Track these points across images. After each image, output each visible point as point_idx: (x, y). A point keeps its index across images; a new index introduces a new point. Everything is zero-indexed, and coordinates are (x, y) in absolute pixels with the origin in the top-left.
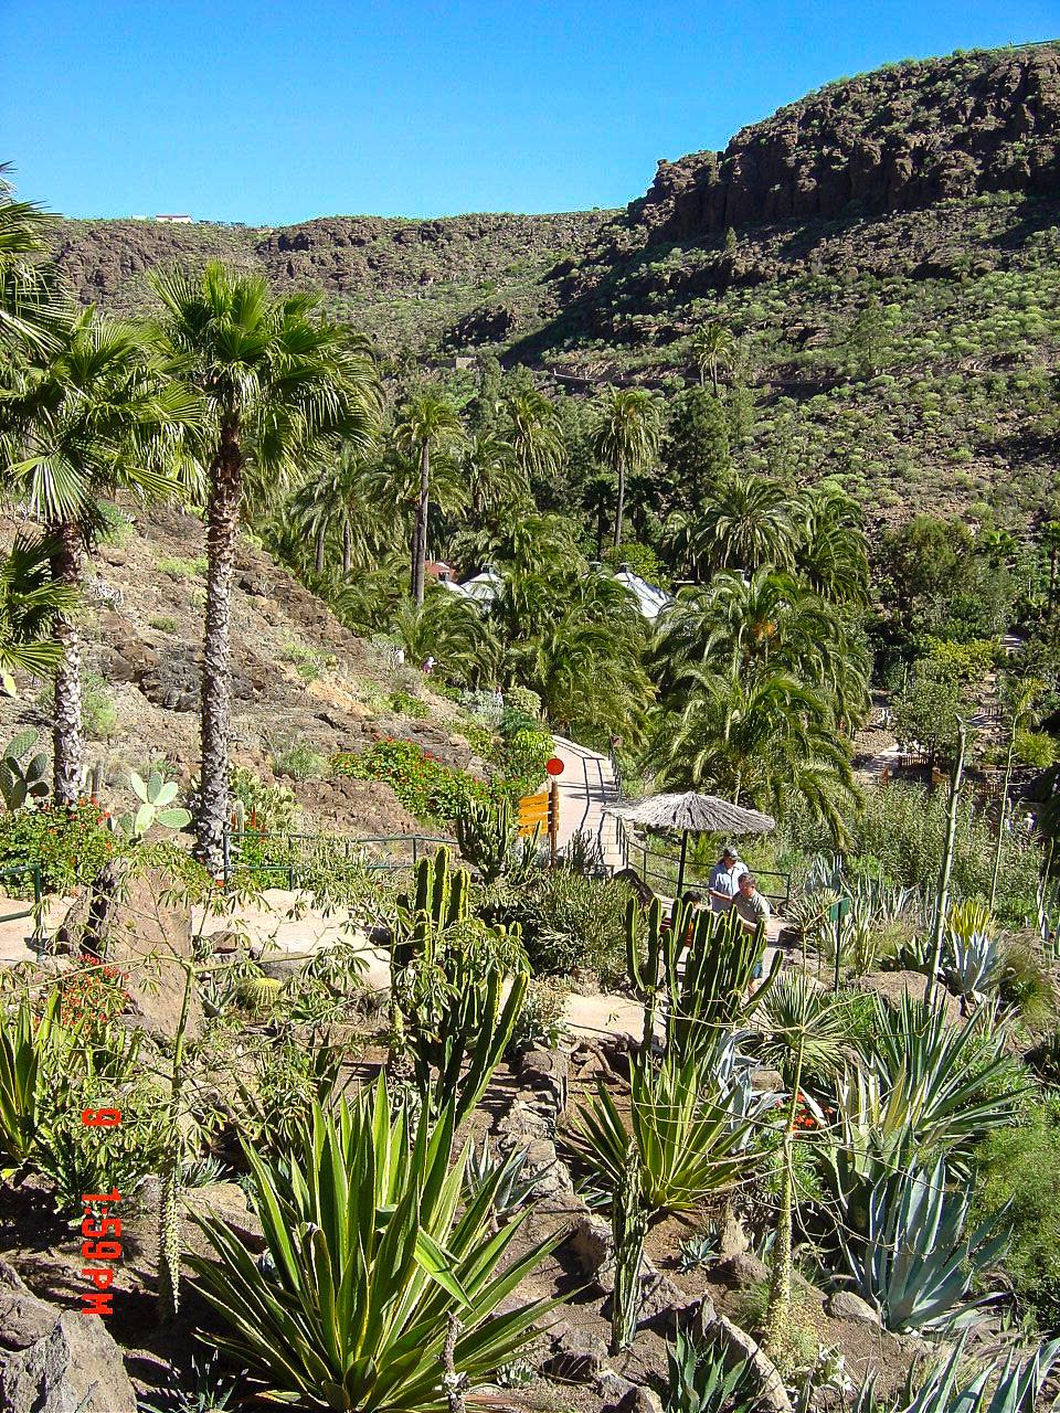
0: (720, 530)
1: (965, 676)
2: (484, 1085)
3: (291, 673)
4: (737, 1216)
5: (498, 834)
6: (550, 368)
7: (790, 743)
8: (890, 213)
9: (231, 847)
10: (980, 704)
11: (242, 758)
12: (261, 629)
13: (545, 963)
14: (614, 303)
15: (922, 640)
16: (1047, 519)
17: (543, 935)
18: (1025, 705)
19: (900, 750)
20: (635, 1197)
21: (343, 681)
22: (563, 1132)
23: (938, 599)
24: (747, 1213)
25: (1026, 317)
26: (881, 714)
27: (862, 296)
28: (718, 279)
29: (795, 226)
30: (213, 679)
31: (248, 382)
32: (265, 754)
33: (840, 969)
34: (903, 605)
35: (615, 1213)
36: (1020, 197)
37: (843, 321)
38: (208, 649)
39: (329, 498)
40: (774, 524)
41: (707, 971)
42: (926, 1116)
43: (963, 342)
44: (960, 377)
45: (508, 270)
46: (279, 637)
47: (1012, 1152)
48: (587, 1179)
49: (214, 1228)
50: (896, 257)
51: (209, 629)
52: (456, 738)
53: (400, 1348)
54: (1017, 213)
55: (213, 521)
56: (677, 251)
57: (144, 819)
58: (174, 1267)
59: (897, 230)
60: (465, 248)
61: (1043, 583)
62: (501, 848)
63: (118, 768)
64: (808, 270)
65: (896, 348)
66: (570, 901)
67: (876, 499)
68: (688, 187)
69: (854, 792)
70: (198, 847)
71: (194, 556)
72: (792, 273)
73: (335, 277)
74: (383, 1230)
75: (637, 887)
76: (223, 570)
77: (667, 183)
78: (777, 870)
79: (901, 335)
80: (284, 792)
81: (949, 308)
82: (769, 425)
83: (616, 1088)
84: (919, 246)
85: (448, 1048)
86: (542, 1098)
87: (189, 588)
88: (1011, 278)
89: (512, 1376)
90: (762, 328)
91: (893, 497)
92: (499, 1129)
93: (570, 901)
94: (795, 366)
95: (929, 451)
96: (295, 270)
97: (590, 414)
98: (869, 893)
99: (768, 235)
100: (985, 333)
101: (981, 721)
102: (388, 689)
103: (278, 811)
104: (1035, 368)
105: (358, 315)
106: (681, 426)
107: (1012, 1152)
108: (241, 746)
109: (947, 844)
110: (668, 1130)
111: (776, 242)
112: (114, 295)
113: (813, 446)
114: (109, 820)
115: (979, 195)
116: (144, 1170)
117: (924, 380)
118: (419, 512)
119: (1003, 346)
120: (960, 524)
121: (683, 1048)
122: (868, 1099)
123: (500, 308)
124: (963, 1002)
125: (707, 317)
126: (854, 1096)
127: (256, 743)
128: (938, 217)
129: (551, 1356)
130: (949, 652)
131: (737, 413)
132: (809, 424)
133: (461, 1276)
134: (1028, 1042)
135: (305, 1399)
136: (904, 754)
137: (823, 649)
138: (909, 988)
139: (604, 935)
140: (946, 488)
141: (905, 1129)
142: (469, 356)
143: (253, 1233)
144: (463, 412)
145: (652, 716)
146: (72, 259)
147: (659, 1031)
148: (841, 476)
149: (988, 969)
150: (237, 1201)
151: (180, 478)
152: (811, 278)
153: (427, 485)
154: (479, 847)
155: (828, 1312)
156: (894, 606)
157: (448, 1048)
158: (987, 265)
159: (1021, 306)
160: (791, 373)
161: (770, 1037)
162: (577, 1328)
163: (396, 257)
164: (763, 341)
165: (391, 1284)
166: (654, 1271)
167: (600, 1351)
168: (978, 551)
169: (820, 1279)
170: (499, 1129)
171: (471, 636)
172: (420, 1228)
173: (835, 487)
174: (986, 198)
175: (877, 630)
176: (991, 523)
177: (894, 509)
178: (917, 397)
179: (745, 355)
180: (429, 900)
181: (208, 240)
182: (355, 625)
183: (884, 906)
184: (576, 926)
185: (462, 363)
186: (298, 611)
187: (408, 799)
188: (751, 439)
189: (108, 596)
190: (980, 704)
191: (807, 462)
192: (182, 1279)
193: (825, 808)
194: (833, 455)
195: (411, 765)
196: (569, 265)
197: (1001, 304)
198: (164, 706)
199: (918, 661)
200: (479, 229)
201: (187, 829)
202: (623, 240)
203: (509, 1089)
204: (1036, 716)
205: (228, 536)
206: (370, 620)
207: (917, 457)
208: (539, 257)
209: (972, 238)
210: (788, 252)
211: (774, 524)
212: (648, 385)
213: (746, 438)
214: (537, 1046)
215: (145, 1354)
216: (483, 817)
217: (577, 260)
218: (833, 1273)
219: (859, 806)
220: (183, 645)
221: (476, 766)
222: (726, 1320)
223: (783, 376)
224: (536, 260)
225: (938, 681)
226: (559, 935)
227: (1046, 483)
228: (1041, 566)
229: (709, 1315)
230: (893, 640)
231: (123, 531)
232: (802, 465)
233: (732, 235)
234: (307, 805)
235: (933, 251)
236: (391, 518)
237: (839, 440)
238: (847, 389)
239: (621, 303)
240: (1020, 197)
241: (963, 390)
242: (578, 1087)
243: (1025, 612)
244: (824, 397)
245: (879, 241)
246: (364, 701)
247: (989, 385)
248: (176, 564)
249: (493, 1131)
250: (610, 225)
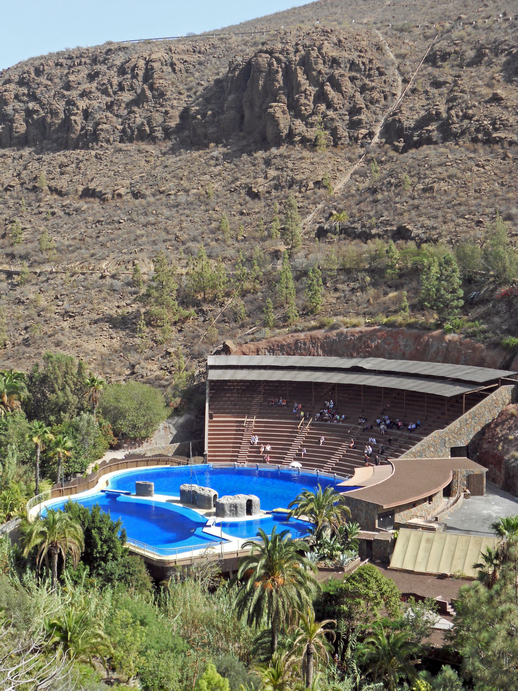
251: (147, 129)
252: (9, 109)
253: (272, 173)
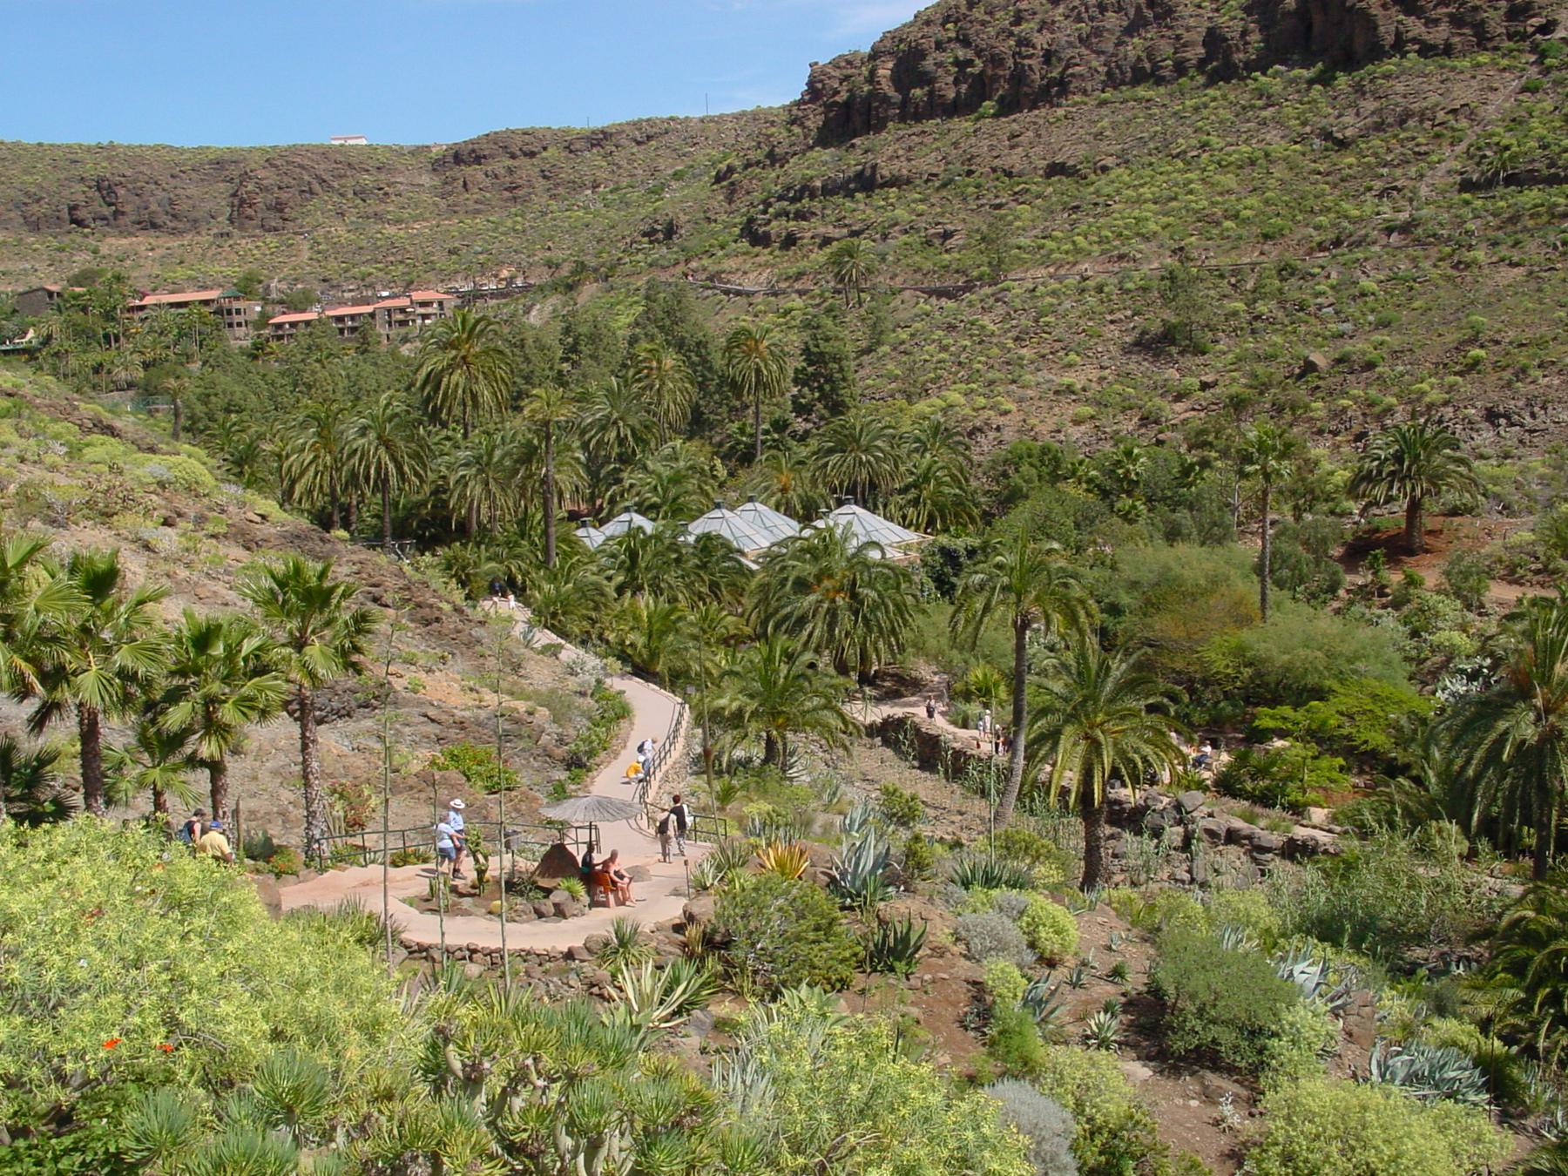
90: (906, 232)
96: (470, 185)
146: (250, 187)
158: (1109, 161)
200: (647, 134)
251: (1147, 66)
252: (928, 64)
253: (1369, 105)
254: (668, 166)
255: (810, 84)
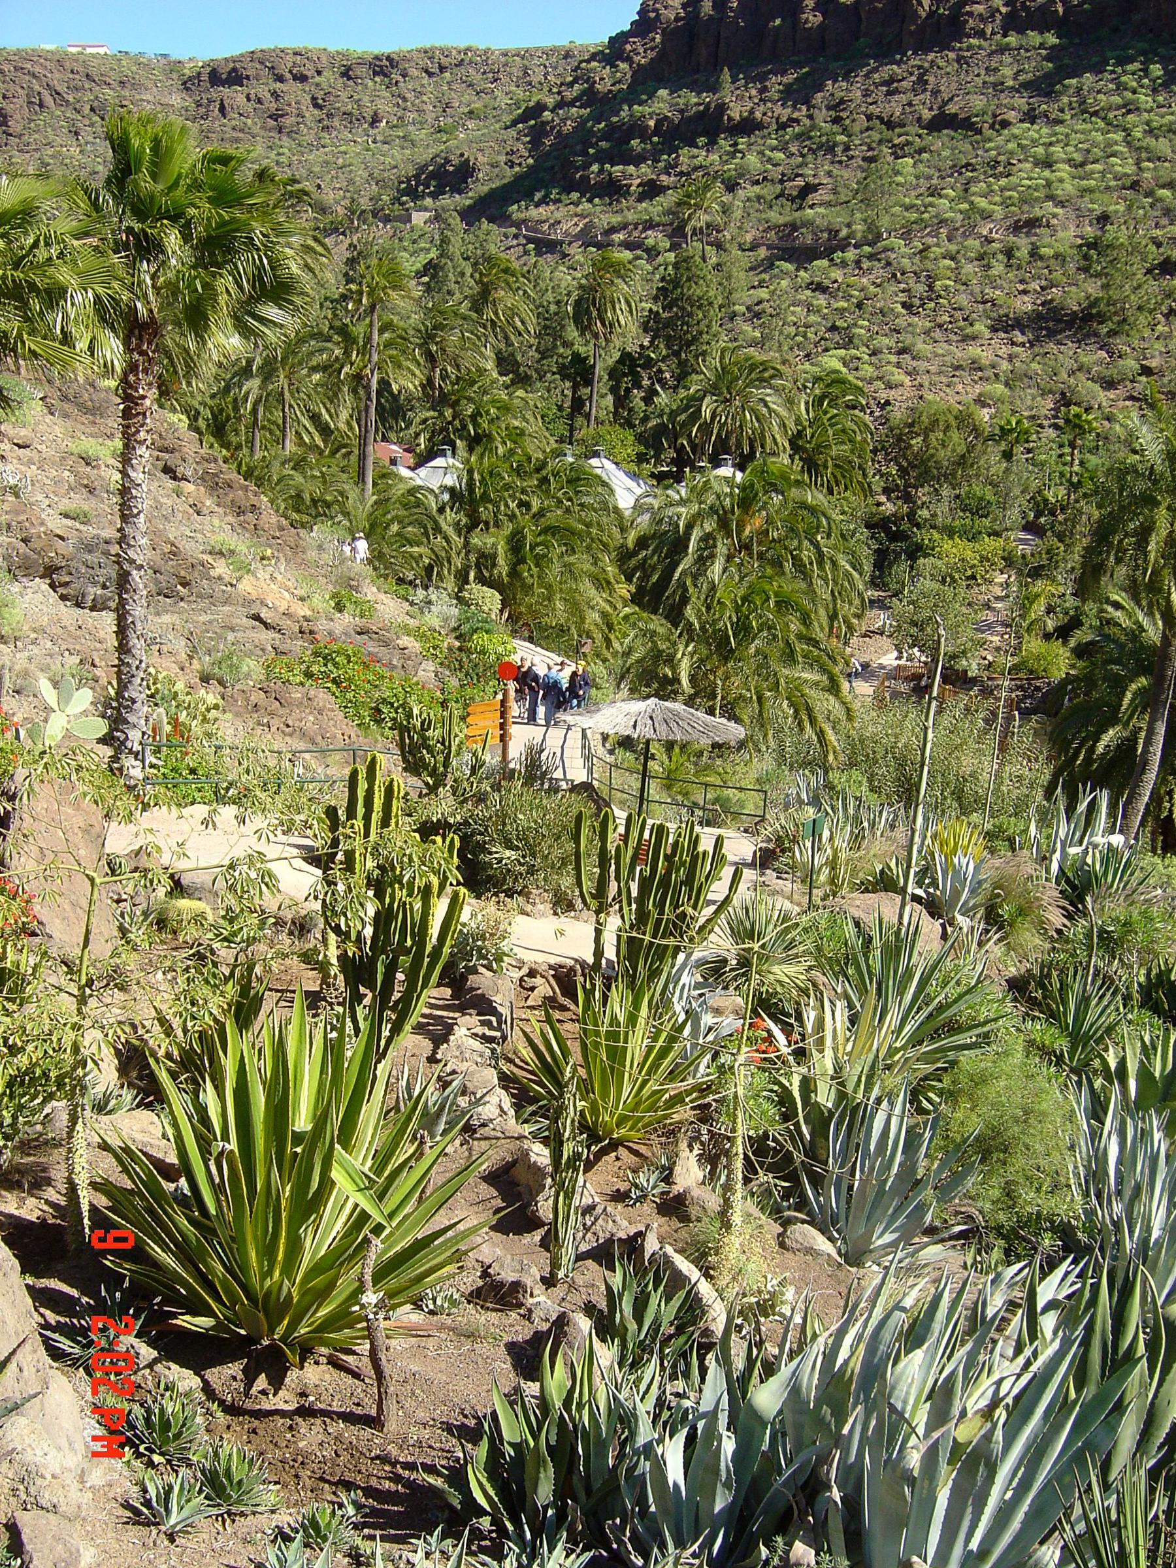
0: (706, 412)
1: (973, 577)
2: (421, 1009)
3: (221, 568)
4: (690, 1147)
5: (443, 744)
6: (517, 224)
7: (774, 652)
8: (904, 54)
9: (150, 759)
10: (989, 608)
11: (165, 662)
12: (182, 517)
13: (478, 877)
14: (591, 151)
15: (923, 536)
16: (1068, 404)
17: (491, 853)
18: (1039, 608)
19: (899, 658)
20: (573, 1121)
21: (279, 578)
22: (510, 1061)
23: (946, 491)
24: (702, 1144)
25: (1053, 177)
26: (879, 618)
27: (870, 149)
28: (709, 126)
29: (798, 65)
30: (129, 574)
31: (172, 239)
32: (191, 657)
33: (815, 891)
34: (908, 498)
35: (554, 1141)
36: (1052, 39)
37: (850, 176)
38: (123, 540)
39: (268, 372)
40: (766, 405)
41: (666, 886)
42: (898, 1045)
43: (982, 203)
44: (977, 243)
45: (471, 112)
46: (208, 528)
47: (981, 1080)
48: (533, 1108)
49: (125, 1156)
50: (910, 104)
51: (125, 518)
52: (405, 641)
53: (317, 1269)
54: (1048, 58)
55: (127, 398)
56: (663, 92)
57: (55, 728)
58: (86, 1197)
59: (911, 74)
60: (423, 86)
61: (1062, 474)
62: (447, 758)
63: (26, 674)
64: (810, 117)
65: (908, 208)
66: (521, 816)
67: (880, 378)
68: (677, 19)
69: (844, 703)
70: (115, 759)
71: (110, 437)
72: (793, 121)
73: (275, 117)
74: (299, 1150)
75: (594, 801)
76: (139, 452)
77: (653, 15)
78: (758, 787)
79: (913, 193)
80: (211, 699)
81: (968, 165)
82: (763, 294)
83: (568, 1015)
84: (936, 93)
85: (381, 969)
86: (487, 1024)
87: (104, 472)
88: (1038, 132)
89: (439, 1302)
90: (757, 183)
91: (899, 376)
92: (438, 1057)
93: (521, 816)
94: (794, 227)
95: (940, 326)
96: (228, 109)
97: (564, 279)
98: (851, 811)
99: (762, 78)
100: (1008, 194)
101: (990, 627)
102: (331, 587)
103: (205, 720)
104: (1061, 234)
105: (300, 162)
106: (669, 292)
107: (981, 1080)
108: (165, 649)
109: (923, 754)
110: (617, 1055)
111: (775, 84)
112: (20, 136)
113: (813, 318)
114: (17, 731)
115: (1005, 36)
116: (50, 1097)
117: (938, 245)
118: (367, 388)
119: (1026, 208)
120: (973, 408)
121: (635, 969)
122: (835, 1030)
123: (462, 155)
124: (943, 926)
125: (696, 169)
126: (820, 1024)
127: (180, 646)
128: (958, 60)
129: (480, 1283)
130: (954, 550)
131: (729, 278)
132: (808, 293)
133: (381, 1196)
134: (1013, 969)
135: (219, 1326)
136: (902, 662)
137: (817, 546)
138: (884, 909)
139: (557, 852)
140: (958, 368)
141: (871, 1056)
142: (426, 209)
143: (168, 1160)
144: (419, 274)
145: (626, 618)
147: (610, 953)
148: (842, 352)
149: (973, 891)
150: (151, 1128)
151: (91, 348)
152: (813, 127)
153: (375, 358)
154: (422, 759)
155: (782, 1245)
156: (898, 498)
157: (381, 969)
158: (1012, 116)
159: (1048, 163)
160: (790, 235)
161: (734, 962)
162: (516, 1258)
163: (344, 96)
164: (759, 198)
165: (309, 1205)
166: (597, 1199)
167: (532, 1278)
168: (991, 437)
169: (776, 1212)
170: (438, 1057)
171: (425, 528)
172: (337, 1146)
173: (836, 365)
174: (1012, 39)
175: (876, 524)
176: (1006, 407)
177: (900, 390)
178: (929, 265)
179: (738, 214)
180: (360, 810)
181: (127, 74)
182: (295, 516)
183: (866, 824)
184: (527, 844)
185: (418, 218)
186: (229, 499)
187: (350, 708)
188: (743, 309)
189: (12, 482)
190: (989, 608)
191: (805, 336)
192: (93, 1209)
193: (813, 721)
194: (833, 328)
195: (353, 670)
196: (540, 107)
197: (1026, 160)
198: (78, 605)
199: (922, 560)
200: (438, 64)
201: (102, 741)
202: (602, 79)
203: (451, 1015)
204: (1049, 622)
205: (144, 414)
206: (308, 509)
207: (927, 332)
208: (507, 97)
209: (995, 85)
210: (790, 95)
211: (766, 405)
212: (628, 245)
213: (737, 307)
214: (482, 970)
215: (55, 1284)
216: (426, 726)
217: (550, 101)
218: (789, 1208)
219: (850, 718)
220: (98, 537)
221: (427, 672)
222: (669, 1250)
223: (781, 239)
224: (503, 101)
225: (943, 582)
226: (508, 853)
227: (1070, 364)
228: (1060, 456)
229: (651, 1245)
230: (895, 537)
231: (30, 409)
232: (799, 339)
233: (726, 75)
234: (237, 714)
235: (951, 99)
236: (336, 395)
237: (841, 311)
238: (851, 254)
239: (600, 151)
240: (1052, 39)
241: (980, 258)
242: (528, 1014)
243: (1041, 506)
244: (824, 263)
245: (891, 86)
246: (302, 599)
247: (1009, 253)
248: (89, 445)
249: (432, 1060)
250: (588, 61)
254: (463, 100)
255: (642, 12)
